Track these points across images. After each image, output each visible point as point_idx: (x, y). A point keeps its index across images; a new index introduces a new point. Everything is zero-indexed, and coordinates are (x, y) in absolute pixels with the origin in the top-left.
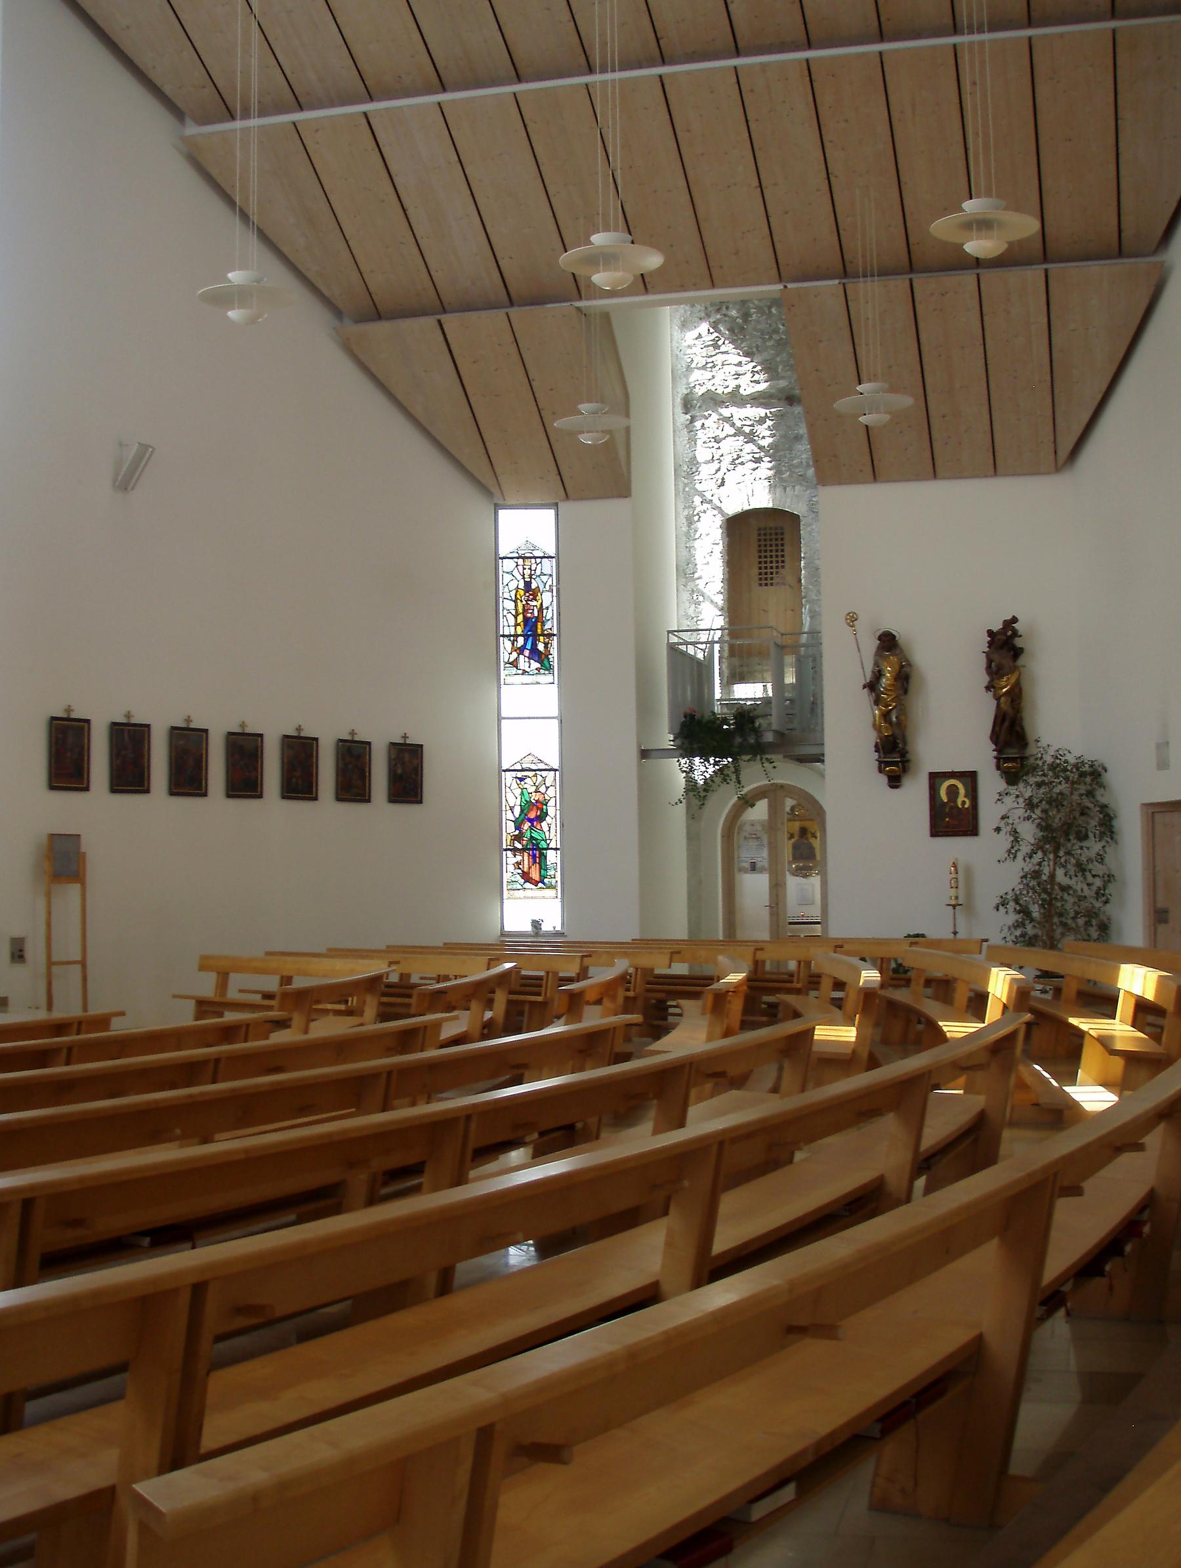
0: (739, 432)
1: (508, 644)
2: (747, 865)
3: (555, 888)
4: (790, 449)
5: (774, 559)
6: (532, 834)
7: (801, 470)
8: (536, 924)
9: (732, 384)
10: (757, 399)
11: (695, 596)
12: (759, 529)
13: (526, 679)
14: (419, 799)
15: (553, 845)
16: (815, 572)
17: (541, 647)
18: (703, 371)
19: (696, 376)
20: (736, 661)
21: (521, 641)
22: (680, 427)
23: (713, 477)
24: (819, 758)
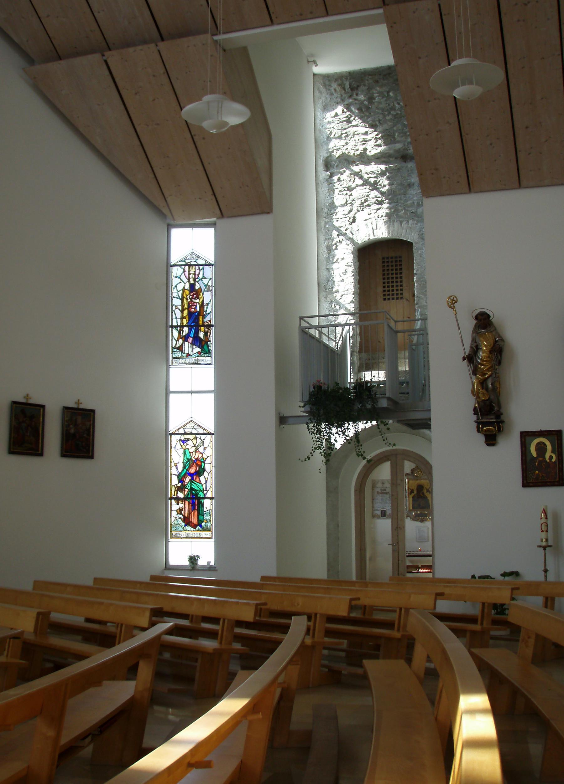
0: (366, 182)
1: (175, 334)
2: (379, 513)
3: (210, 530)
4: (405, 194)
5: (395, 280)
6: (193, 486)
7: (413, 208)
8: (193, 560)
9: (361, 148)
10: (378, 159)
11: (333, 305)
12: (383, 258)
13: (188, 360)
14: (91, 455)
15: (209, 495)
16: (423, 286)
17: (202, 335)
18: (338, 140)
19: (333, 144)
20: (364, 355)
21: (186, 330)
22: (322, 181)
23: (347, 216)
24: (426, 424)
